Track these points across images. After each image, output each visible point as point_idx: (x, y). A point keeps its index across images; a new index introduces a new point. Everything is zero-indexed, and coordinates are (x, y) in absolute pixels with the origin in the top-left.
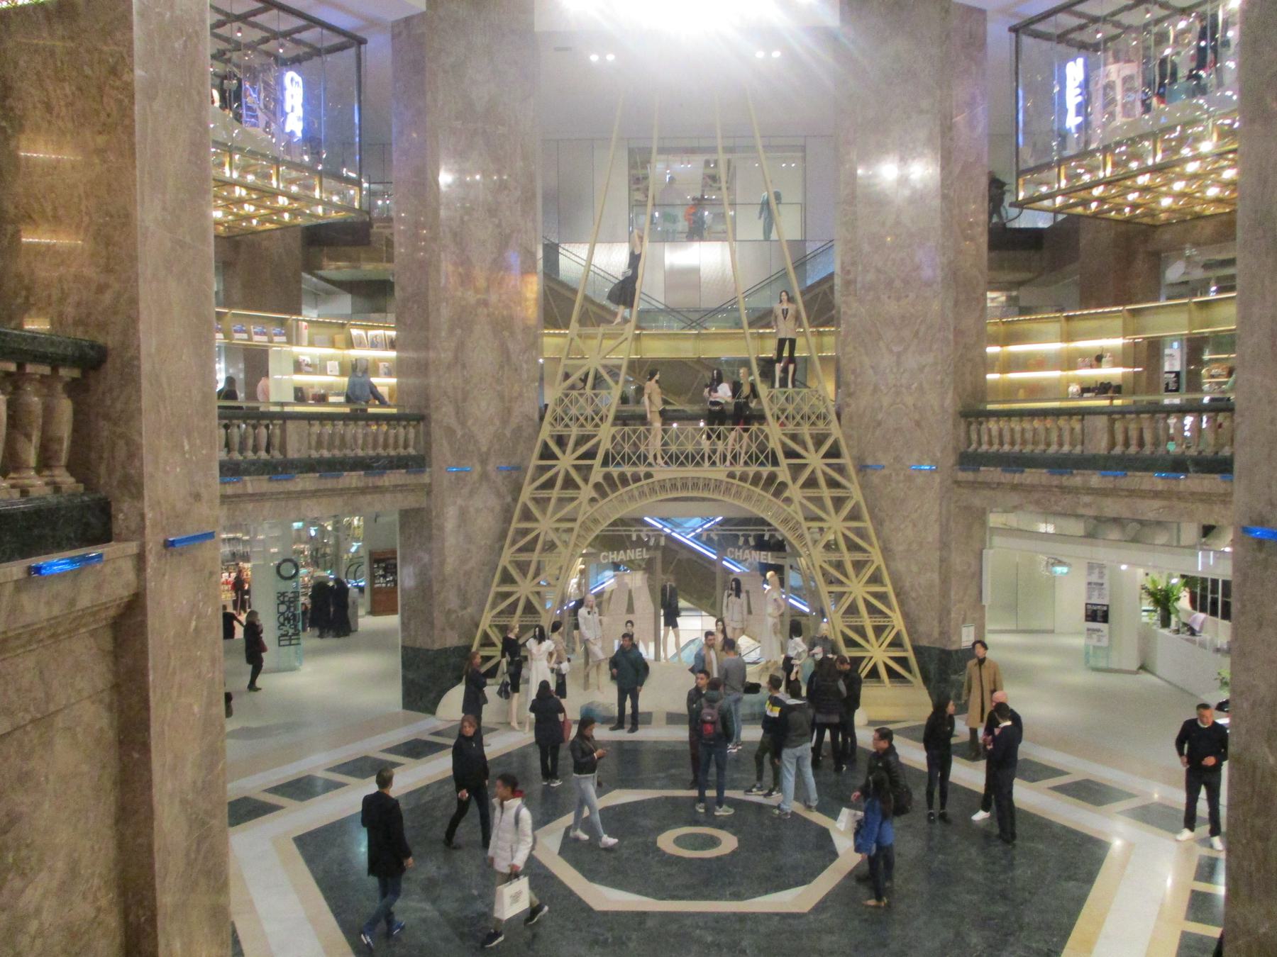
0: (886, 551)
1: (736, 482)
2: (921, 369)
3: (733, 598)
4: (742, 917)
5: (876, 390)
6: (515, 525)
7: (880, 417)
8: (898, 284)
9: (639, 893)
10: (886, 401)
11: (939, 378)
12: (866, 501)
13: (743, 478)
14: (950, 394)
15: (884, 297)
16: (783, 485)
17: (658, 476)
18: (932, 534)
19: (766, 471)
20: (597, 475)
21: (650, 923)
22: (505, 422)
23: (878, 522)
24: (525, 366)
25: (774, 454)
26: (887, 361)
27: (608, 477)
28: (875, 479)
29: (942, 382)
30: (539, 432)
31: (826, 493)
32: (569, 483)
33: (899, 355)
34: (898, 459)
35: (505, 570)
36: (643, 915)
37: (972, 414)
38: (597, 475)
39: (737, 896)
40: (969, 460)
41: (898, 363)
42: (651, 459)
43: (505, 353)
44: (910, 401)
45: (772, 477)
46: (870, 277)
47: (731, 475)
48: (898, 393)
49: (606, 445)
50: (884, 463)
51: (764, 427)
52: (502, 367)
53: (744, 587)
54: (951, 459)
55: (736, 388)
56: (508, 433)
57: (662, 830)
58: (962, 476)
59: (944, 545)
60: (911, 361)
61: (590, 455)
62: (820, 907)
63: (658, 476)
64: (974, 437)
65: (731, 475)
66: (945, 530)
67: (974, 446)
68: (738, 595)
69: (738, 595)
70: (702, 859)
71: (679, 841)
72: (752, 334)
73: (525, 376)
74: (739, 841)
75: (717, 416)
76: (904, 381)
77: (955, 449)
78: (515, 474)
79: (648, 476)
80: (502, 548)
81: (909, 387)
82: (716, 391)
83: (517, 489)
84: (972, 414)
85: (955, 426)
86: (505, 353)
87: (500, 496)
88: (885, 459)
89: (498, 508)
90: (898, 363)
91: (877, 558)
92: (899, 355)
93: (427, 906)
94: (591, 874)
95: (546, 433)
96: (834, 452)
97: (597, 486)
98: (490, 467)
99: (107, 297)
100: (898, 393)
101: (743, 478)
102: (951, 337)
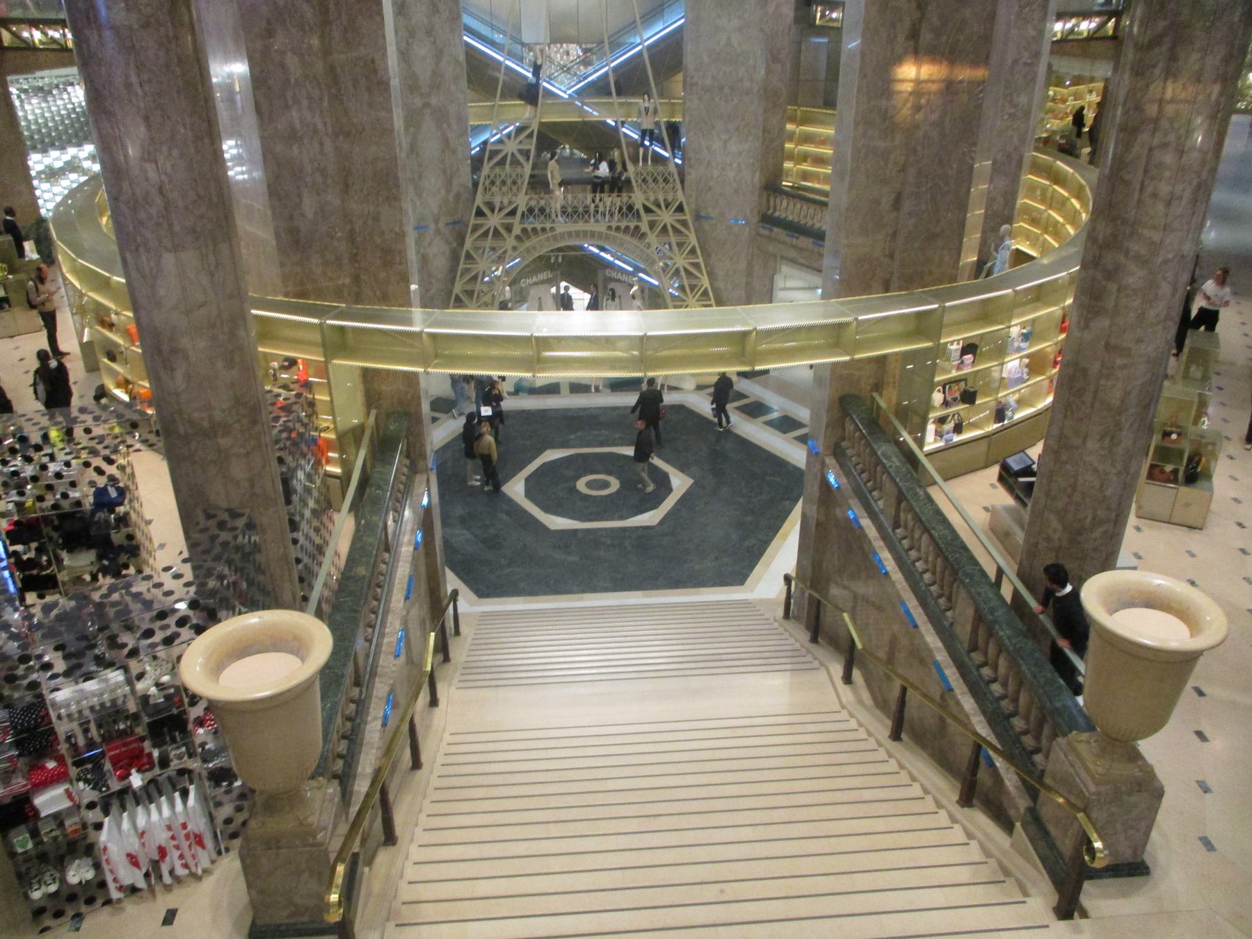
0: (711, 275)
1: (613, 233)
2: (740, 154)
3: (610, 301)
4: (624, 530)
5: (709, 164)
6: (462, 266)
7: (711, 184)
8: (727, 90)
9: (571, 518)
10: (716, 173)
11: (751, 161)
12: (699, 243)
13: (618, 229)
14: (757, 175)
15: (717, 99)
16: (643, 235)
17: (559, 230)
18: (743, 265)
19: (632, 225)
20: (517, 230)
21: (580, 535)
22: (448, 191)
23: (707, 255)
24: (460, 149)
25: (638, 210)
26: (717, 145)
27: (524, 230)
28: (706, 225)
29: (753, 164)
30: (474, 200)
31: (673, 239)
32: (497, 234)
33: (725, 142)
34: (722, 214)
35: (457, 295)
36: (575, 531)
37: (772, 187)
38: (517, 230)
39: (622, 518)
40: (768, 220)
41: (725, 148)
42: (553, 216)
43: (446, 141)
44: (731, 174)
45: (637, 228)
46: (708, 81)
47: (610, 228)
48: (724, 169)
49: (522, 208)
50: (712, 215)
51: (632, 195)
52: (443, 151)
53: (617, 294)
54: (755, 219)
55: (612, 165)
56: (451, 198)
57: (578, 477)
58: (762, 231)
59: (750, 273)
60: (733, 147)
61: (512, 213)
62: (662, 522)
63: (559, 230)
64: (772, 204)
65: (610, 228)
66: (750, 265)
67: (770, 212)
68: (613, 299)
69: (613, 299)
70: (601, 496)
71: (589, 485)
72: (619, 103)
73: (460, 156)
74: (621, 483)
75: (598, 186)
76: (728, 161)
77: (759, 212)
78: (457, 227)
79: (552, 229)
80: (455, 277)
81: (731, 165)
82: (598, 169)
83: (461, 240)
84: (772, 187)
85: (760, 196)
86: (446, 141)
87: (448, 243)
88: (713, 213)
89: (448, 252)
90: (725, 148)
91: (705, 282)
92: (725, 142)
93: (465, 532)
94: (547, 509)
95: (479, 200)
96: (680, 209)
97: (518, 238)
98: (441, 224)
99: (409, 395)
100: (724, 169)
101: (618, 229)
102: (760, 134)
